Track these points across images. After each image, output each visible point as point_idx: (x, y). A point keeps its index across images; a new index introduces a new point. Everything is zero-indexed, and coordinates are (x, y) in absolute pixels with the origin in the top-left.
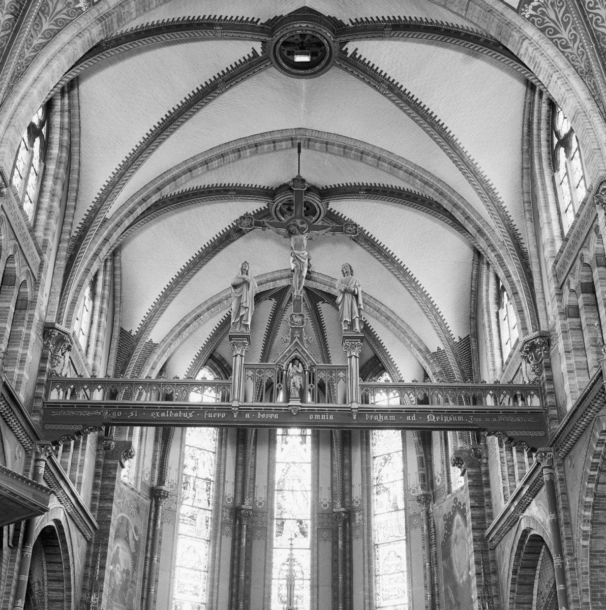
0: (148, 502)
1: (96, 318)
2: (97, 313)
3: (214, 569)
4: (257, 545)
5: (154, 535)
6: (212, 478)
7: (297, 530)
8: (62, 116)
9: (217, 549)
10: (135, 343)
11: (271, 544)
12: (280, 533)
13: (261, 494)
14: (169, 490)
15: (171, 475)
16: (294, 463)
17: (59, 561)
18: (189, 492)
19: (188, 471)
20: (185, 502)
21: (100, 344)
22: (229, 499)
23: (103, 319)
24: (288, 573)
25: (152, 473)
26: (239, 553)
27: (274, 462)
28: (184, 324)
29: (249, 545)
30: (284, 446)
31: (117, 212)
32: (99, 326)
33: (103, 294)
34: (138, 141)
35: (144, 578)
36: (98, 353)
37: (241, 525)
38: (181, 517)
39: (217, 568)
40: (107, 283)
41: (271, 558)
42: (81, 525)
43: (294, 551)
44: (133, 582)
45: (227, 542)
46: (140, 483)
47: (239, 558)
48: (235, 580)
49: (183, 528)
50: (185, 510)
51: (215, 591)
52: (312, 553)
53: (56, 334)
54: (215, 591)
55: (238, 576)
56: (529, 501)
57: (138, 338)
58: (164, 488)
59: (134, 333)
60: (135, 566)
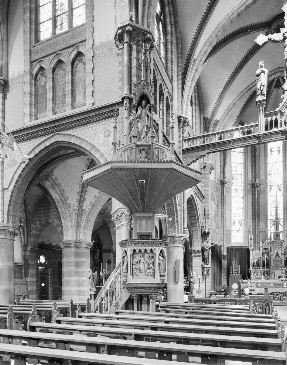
0: (220, 186)
1: (194, 114)
2: (194, 111)
3: (246, 207)
4: (262, 197)
5: (223, 198)
6: (243, 174)
7: (277, 189)
8: (169, 8)
9: (247, 200)
10: (210, 122)
11: (267, 195)
12: (270, 191)
13: (262, 177)
14: (227, 180)
15: (227, 175)
16: (275, 163)
17: (193, 209)
18: (234, 181)
19: (233, 173)
20: (233, 184)
21: (197, 125)
22: (250, 181)
23: (197, 114)
24: (275, 205)
25: (221, 175)
26: (255, 200)
27: (267, 163)
28: (229, 109)
29: (258, 197)
30: (271, 156)
31: (199, 54)
32: (196, 117)
33: (195, 102)
34: (202, 15)
35: (221, 213)
36: (197, 129)
37: (255, 190)
38: (232, 190)
39: (247, 207)
40: (196, 97)
41: (267, 201)
42: (199, 196)
43: (277, 197)
44: (218, 215)
45: (250, 197)
46: (216, 179)
47: (255, 202)
48: (254, 210)
49: (233, 194)
50: (233, 187)
51: (247, 215)
52: (284, 197)
53: (182, 119)
54: (247, 215)
55: (255, 209)
56: (48, 248)
57: (211, 120)
58: (225, 180)
59: (209, 118)
60: (218, 209)
